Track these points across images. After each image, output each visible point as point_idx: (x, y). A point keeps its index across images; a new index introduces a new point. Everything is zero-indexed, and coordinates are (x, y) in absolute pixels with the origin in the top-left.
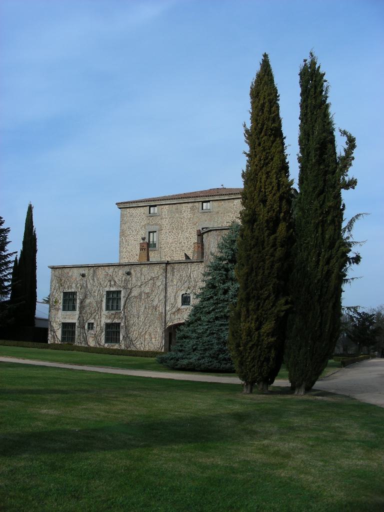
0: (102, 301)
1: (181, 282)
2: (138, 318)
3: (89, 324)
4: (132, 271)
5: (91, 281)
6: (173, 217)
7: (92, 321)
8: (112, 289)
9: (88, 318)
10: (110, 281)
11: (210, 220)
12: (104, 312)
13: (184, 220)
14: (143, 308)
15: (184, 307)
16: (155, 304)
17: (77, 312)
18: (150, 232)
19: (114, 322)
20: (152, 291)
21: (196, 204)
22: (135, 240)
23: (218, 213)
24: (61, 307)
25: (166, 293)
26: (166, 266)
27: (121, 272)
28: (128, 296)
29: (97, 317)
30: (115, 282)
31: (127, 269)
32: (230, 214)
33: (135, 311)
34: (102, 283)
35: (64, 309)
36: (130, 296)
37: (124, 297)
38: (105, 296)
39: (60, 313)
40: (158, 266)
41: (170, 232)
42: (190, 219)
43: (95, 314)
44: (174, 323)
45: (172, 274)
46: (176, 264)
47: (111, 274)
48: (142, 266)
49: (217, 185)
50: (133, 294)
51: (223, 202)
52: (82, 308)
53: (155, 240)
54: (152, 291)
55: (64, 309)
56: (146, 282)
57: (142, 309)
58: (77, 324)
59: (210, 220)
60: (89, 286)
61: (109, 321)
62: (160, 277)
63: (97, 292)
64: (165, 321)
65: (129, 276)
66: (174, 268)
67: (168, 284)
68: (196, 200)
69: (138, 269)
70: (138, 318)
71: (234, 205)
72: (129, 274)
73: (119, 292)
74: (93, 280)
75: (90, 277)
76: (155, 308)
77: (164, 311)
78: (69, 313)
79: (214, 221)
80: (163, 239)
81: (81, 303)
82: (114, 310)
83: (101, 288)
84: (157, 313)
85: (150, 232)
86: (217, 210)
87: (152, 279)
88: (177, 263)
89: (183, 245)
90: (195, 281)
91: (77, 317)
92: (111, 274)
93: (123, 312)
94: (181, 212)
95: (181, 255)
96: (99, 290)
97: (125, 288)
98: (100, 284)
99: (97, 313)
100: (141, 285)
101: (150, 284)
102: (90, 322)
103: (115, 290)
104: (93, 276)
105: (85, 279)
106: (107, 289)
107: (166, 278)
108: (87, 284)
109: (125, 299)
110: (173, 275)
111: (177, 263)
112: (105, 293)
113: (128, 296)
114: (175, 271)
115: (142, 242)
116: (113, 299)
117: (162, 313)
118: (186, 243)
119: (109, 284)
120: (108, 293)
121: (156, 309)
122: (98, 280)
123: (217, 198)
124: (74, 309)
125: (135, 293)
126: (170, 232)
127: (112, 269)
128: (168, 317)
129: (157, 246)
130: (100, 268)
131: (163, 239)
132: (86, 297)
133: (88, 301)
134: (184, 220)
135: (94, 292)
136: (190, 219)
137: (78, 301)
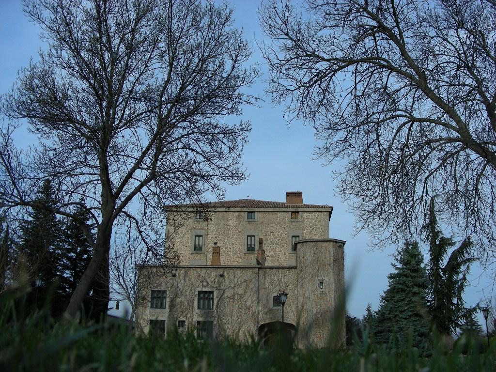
0: (194, 300)
1: (272, 285)
2: (231, 317)
3: (179, 321)
4: (225, 274)
5: (183, 281)
6: (219, 224)
7: (184, 319)
8: (204, 289)
9: (179, 316)
10: (202, 282)
11: (255, 229)
12: (196, 311)
13: (230, 227)
14: (236, 308)
15: (275, 308)
16: (248, 304)
17: (167, 310)
18: (196, 236)
19: (206, 320)
20: (245, 292)
21: (242, 214)
22: (181, 243)
23: (262, 223)
24: (149, 304)
25: (258, 295)
26: (259, 270)
27: (214, 274)
28: (222, 296)
29: (189, 315)
30: (208, 283)
31: (220, 271)
32: (273, 225)
33: (228, 311)
34: (194, 283)
35: (151, 307)
36: (224, 296)
37: (217, 297)
38: (197, 296)
39: (148, 311)
40: (251, 270)
41: (216, 237)
42: (236, 227)
43: (186, 312)
44: (266, 322)
45: (263, 278)
46: (268, 269)
47: (204, 275)
48: (235, 270)
49: (243, 197)
50: (226, 295)
51: (267, 214)
52: (172, 306)
53: (200, 244)
54: (245, 292)
55: (151, 307)
56: (238, 285)
57: (236, 308)
58: (166, 322)
59: (255, 229)
60: (179, 285)
61: (201, 319)
62: (253, 280)
63: (188, 292)
64: (258, 320)
65: (222, 278)
66: (265, 273)
67: (260, 287)
68: (243, 210)
69: (231, 272)
70: (231, 317)
71: (277, 217)
72: (222, 276)
73: (212, 292)
74: (185, 280)
75: (181, 277)
76: (248, 308)
77: (257, 311)
78: (158, 310)
79: (258, 230)
80: (209, 244)
81: (172, 301)
82: (206, 309)
83: (193, 288)
84: (251, 313)
85: (196, 236)
86: (261, 220)
87: (245, 281)
88: (269, 268)
89: (229, 249)
90: (285, 284)
91: (167, 314)
92: (204, 275)
93: (216, 311)
94: (228, 220)
95: (226, 259)
96: (191, 290)
97: (217, 288)
98: (192, 284)
99: (189, 312)
100: (235, 287)
101: (243, 287)
102: (181, 320)
103: (208, 290)
104: (185, 277)
105: (175, 278)
106: (200, 289)
107: (258, 281)
108: (178, 284)
109: (218, 299)
110: (265, 279)
111: (269, 268)
112: (197, 293)
113: (222, 296)
114: (267, 275)
115: (213, 245)
116: (205, 297)
117: (255, 312)
118: (232, 249)
119: (201, 284)
120: (200, 293)
121: (249, 309)
122: (189, 280)
123: (271, 210)
124: (162, 307)
125: (228, 293)
126: (216, 237)
127: (204, 271)
128: (260, 316)
129: (203, 249)
130: (191, 269)
131: (209, 244)
132: (176, 296)
133: (178, 300)
134: (230, 227)
135: (186, 291)
136: (236, 227)
137: (168, 300)
